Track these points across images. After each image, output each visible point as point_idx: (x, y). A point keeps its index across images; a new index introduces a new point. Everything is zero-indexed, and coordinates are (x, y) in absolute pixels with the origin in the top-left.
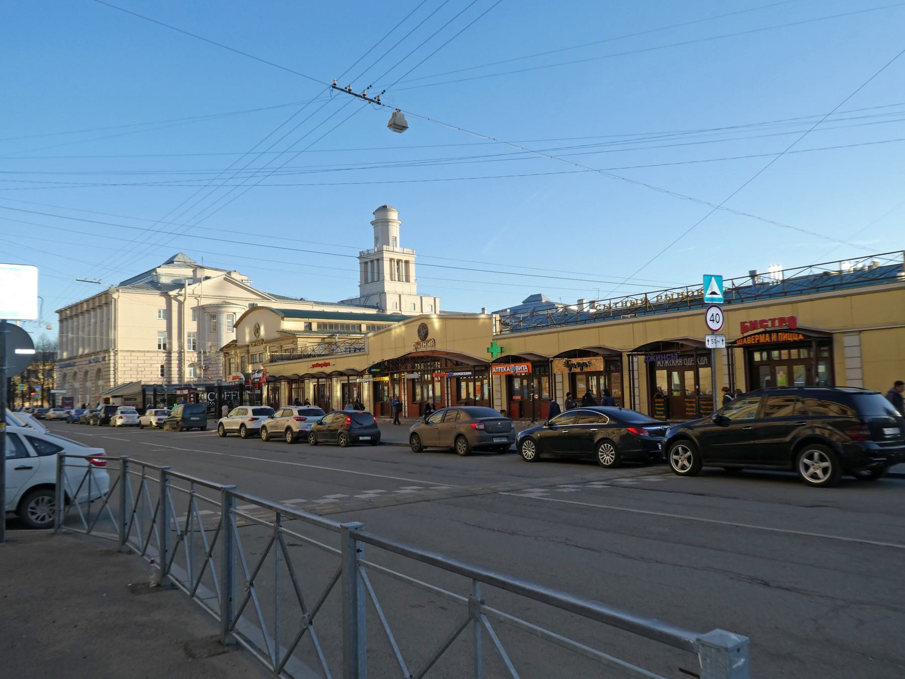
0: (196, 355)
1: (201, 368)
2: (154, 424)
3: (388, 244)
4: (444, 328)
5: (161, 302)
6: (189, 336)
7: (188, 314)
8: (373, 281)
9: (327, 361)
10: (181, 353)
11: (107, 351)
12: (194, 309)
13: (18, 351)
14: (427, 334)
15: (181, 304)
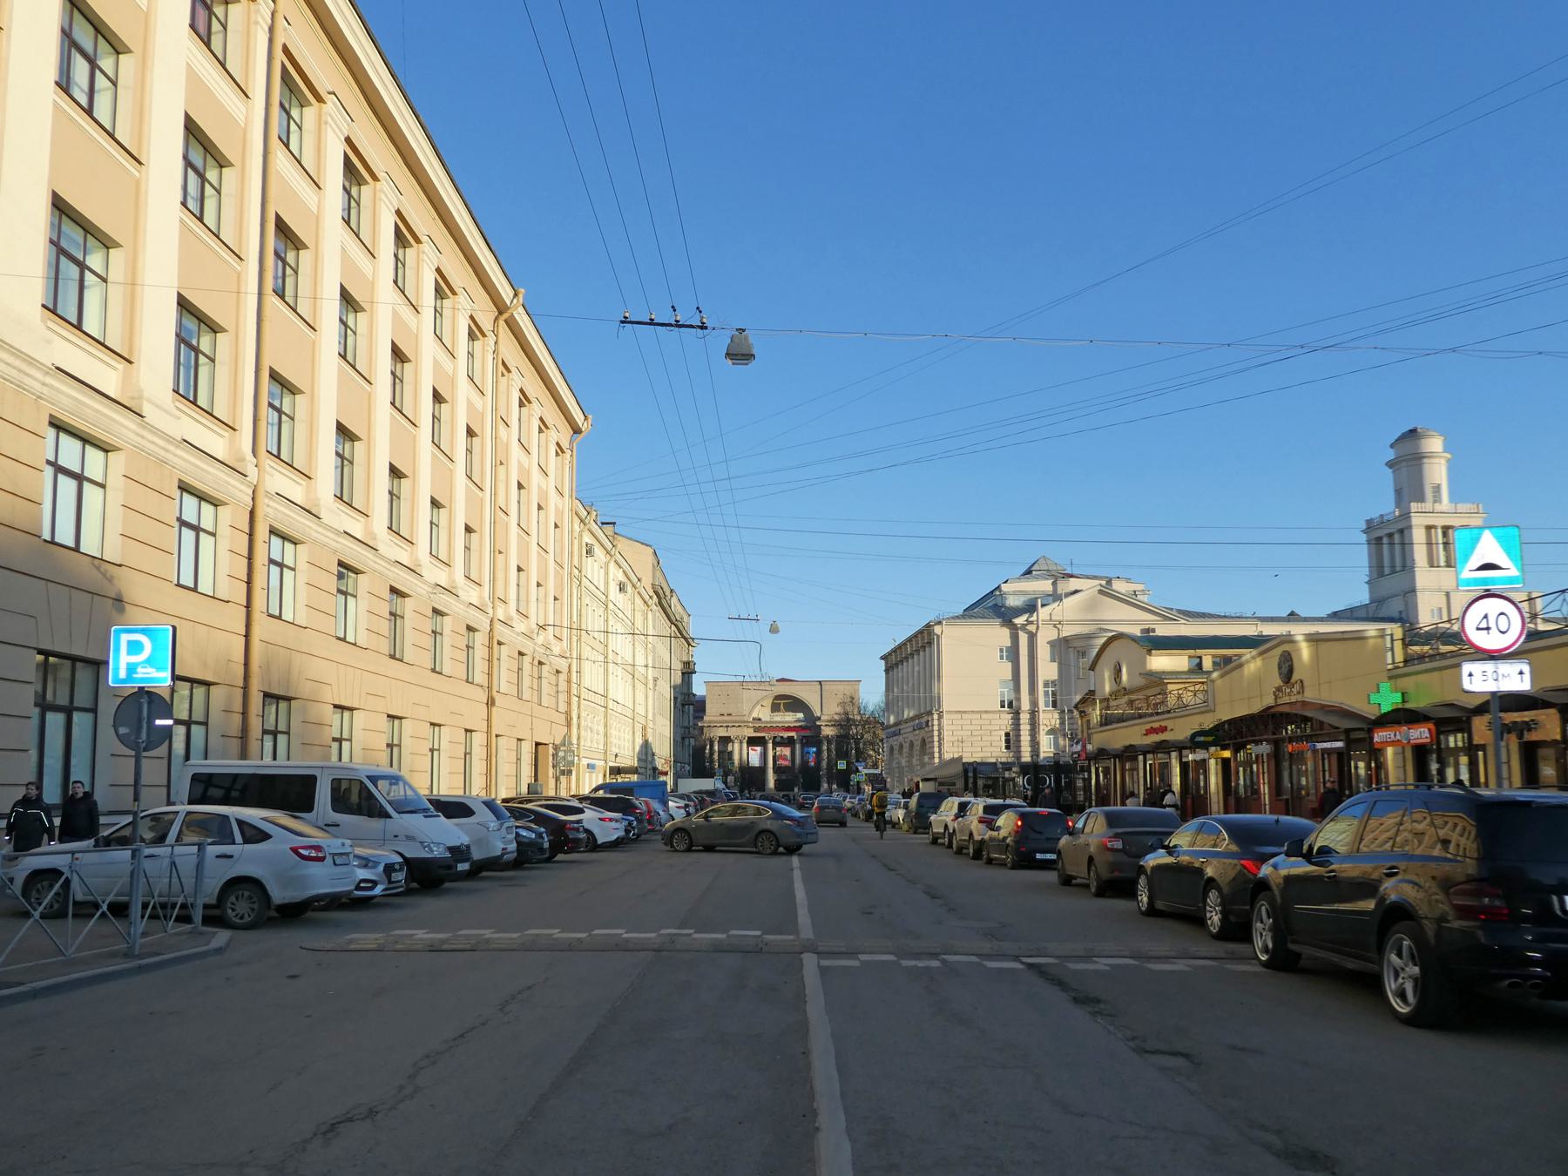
0: (1056, 716)
1: (1065, 736)
2: (933, 817)
3: (1421, 499)
4: (1316, 656)
5: (1002, 636)
6: (1046, 685)
7: (1043, 652)
8: (1393, 572)
9: (1163, 724)
10: (1034, 713)
11: (930, 713)
12: (1052, 644)
13: (158, 722)
14: (1291, 671)
15: (1032, 637)
